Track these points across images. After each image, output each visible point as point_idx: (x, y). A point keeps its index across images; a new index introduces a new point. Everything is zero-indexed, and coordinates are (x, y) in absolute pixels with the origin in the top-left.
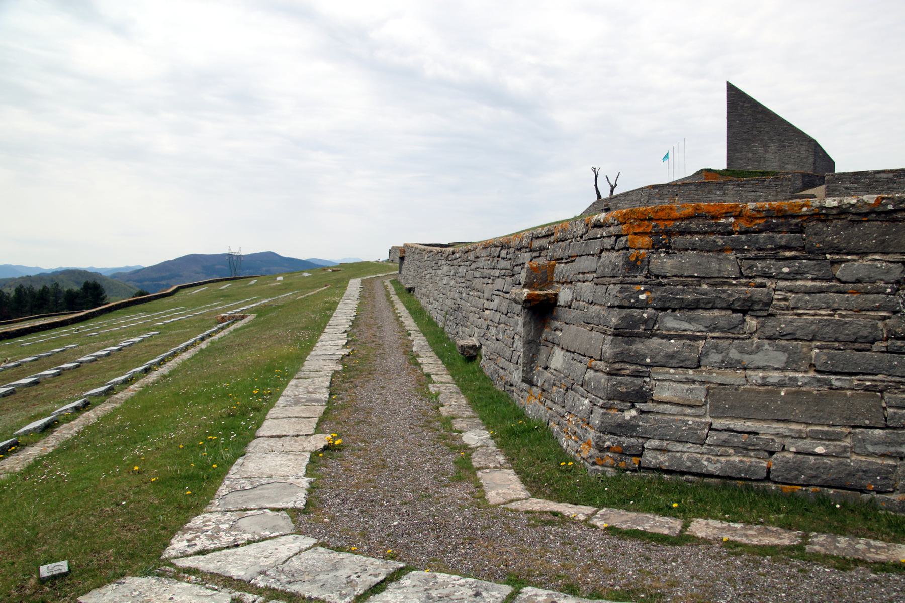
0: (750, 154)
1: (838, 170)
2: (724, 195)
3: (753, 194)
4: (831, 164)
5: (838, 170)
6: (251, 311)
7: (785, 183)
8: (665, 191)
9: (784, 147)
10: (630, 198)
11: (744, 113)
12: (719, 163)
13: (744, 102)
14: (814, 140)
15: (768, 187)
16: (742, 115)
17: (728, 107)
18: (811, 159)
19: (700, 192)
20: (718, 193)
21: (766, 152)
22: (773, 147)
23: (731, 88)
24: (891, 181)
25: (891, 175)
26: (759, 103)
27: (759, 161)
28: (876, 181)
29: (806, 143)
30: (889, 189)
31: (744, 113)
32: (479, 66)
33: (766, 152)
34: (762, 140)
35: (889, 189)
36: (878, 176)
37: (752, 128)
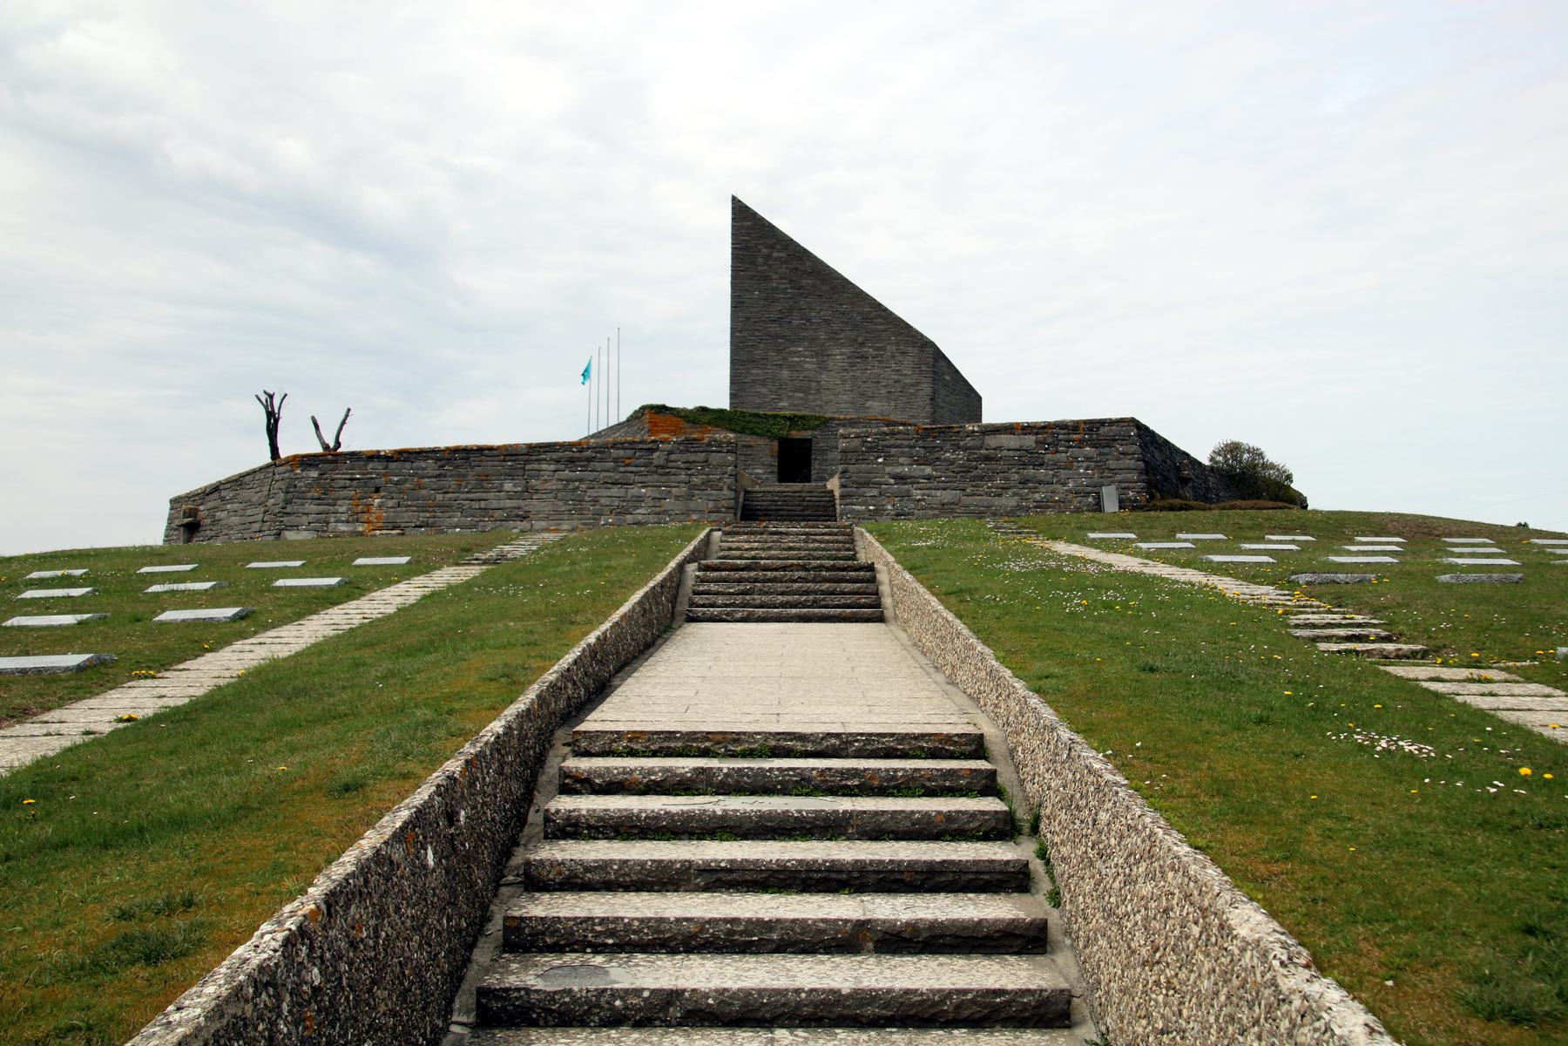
0: (785, 373)
1: (991, 414)
2: (528, 491)
3: (615, 491)
4: (971, 401)
5: (991, 414)
6: (1093, 544)
7: (715, 458)
8: (341, 475)
9: (864, 357)
10: (245, 494)
11: (772, 273)
12: (709, 387)
13: (772, 247)
14: (932, 344)
15: (664, 469)
16: (767, 278)
17: (735, 257)
18: (926, 388)
19: (451, 483)
20: (508, 486)
21: (822, 367)
22: (839, 355)
23: (742, 215)
24: (1029, 459)
25: (1029, 441)
26: (806, 251)
27: (806, 391)
28: (988, 459)
29: (913, 351)
30: (1024, 482)
31: (772, 273)
32: (295, 153)
33: (822, 367)
34: (813, 340)
35: (1024, 482)
36: (992, 441)
37: (790, 310)
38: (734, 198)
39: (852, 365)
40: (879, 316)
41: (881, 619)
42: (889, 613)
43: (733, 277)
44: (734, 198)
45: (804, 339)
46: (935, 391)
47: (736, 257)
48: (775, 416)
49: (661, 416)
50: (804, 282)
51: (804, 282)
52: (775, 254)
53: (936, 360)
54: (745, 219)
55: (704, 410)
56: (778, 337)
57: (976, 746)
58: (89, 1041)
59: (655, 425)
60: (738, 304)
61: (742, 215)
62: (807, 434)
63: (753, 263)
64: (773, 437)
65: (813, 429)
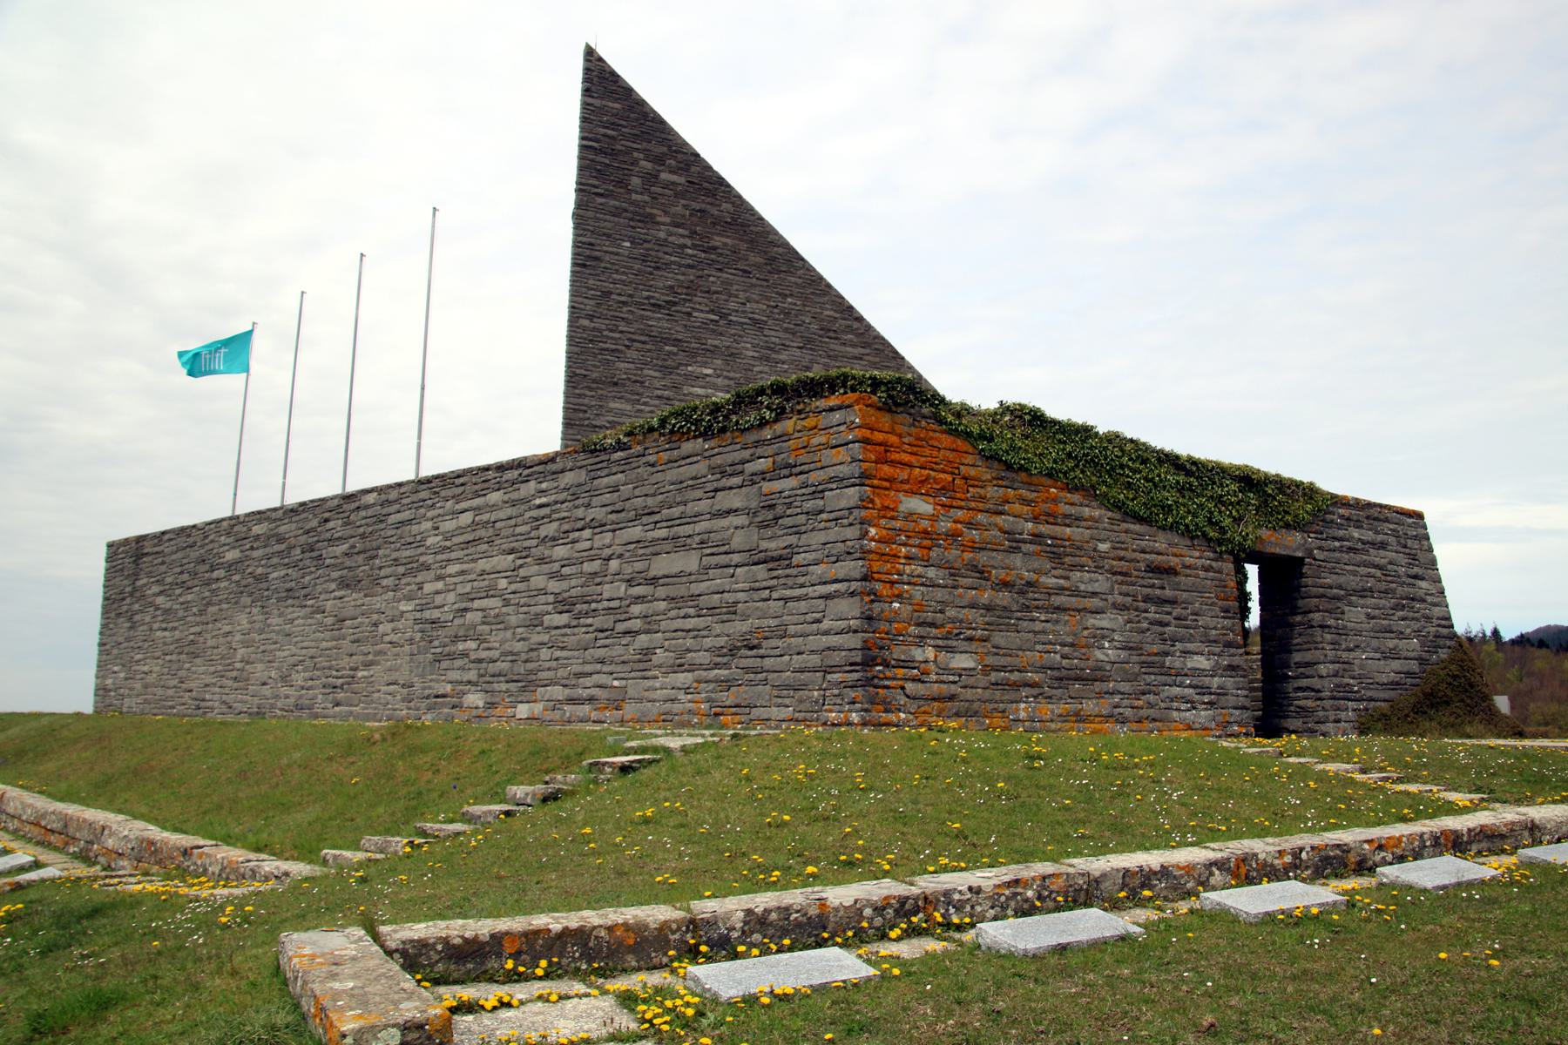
26: (721, 182)
31: (645, 195)
34: (732, 356)
37: (691, 288)
38: (590, 53)
40: (849, 329)
44: (590, 53)
45: (714, 351)
50: (718, 241)
52: (664, 176)
56: (666, 341)
58: (191, 1044)
59: (884, 454)
60: (585, 261)
63: (622, 183)
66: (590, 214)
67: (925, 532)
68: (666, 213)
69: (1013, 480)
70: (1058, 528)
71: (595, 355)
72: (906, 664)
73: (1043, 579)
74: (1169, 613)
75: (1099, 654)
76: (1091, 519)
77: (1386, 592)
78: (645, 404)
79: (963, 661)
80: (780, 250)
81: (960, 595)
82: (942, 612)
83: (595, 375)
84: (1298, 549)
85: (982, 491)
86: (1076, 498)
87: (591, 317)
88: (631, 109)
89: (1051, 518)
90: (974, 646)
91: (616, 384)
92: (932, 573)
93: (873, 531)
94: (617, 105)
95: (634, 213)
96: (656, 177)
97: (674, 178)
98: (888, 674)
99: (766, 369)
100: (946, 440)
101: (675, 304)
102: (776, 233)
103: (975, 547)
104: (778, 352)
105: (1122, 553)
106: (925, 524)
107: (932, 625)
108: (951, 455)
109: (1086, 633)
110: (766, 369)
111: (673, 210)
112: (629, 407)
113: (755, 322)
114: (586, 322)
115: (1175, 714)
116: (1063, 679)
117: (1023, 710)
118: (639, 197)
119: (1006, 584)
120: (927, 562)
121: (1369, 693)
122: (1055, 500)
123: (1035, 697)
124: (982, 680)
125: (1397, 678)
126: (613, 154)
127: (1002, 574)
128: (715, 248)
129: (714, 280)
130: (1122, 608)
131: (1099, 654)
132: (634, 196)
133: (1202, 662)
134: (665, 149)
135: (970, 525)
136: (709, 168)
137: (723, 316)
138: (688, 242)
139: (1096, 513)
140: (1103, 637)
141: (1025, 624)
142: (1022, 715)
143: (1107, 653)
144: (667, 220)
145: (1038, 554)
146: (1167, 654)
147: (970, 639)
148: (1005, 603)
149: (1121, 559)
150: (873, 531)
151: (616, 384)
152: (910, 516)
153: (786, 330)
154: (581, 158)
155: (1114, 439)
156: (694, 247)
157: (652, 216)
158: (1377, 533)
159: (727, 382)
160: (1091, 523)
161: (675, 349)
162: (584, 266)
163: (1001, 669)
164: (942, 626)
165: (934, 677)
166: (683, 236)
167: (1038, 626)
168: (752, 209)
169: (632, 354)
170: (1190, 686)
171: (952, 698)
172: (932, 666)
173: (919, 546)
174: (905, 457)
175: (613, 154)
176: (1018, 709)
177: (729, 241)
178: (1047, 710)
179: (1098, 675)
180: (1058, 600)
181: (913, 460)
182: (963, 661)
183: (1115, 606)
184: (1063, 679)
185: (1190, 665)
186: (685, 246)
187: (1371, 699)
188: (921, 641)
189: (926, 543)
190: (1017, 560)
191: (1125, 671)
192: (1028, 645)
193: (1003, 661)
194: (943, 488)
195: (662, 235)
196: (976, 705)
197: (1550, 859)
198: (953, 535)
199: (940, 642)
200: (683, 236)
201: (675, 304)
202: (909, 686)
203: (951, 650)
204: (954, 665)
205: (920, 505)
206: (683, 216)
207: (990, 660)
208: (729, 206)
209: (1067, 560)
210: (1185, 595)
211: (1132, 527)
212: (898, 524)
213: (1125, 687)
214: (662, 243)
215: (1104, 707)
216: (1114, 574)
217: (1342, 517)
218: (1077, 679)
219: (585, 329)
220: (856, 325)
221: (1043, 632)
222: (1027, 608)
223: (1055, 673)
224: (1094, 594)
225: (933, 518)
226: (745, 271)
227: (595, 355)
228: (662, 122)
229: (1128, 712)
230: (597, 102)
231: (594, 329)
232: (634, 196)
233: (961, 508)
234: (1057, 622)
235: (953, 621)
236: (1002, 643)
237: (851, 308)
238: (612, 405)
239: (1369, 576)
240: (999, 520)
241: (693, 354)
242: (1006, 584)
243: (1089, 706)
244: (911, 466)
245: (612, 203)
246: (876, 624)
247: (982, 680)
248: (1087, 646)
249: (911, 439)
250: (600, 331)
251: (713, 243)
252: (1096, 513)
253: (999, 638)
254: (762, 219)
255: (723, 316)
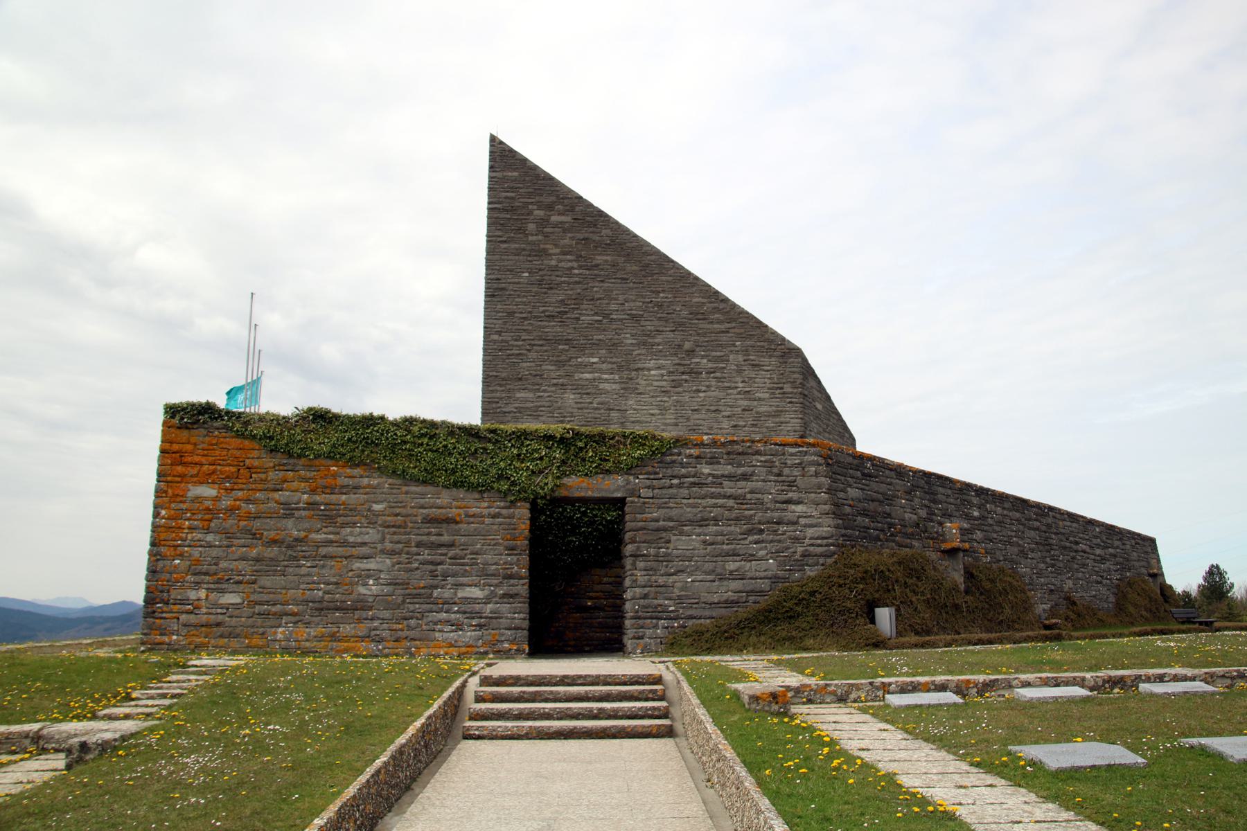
0: (570, 397)
9: (694, 373)
14: (797, 352)
17: (493, 223)
21: (629, 388)
22: (655, 371)
23: (505, 163)
26: (601, 214)
29: (770, 362)
33: (629, 388)
34: (614, 346)
37: (579, 299)
39: (676, 384)
40: (716, 310)
41: (669, 733)
42: (679, 727)
43: (490, 252)
45: (599, 344)
46: (805, 425)
47: (494, 222)
48: (522, 436)
49: (198, 435)
50: (599, 259)
51: (599, 259)
52: (555, 218)
53: (805, 378)
54: (509, 167)
55: (320, 418)
56: (559, 342)
57: (658, 680)
60: (494, 291)
61: (505, 163)
62: (612, 486)
63: (522, 230)
64: (514, 494)
65: (630, 470)
66: (497, 257)
67: (208, 509)
68: (556, 246)
69: (295, 465)
70: (333, 496)
71: (504, 360)
72: (184, 602)
73: (313, 536)
74: (445, 555)
75: (362, 590)
76: (369, 486)
77: (737, 519)
78: (544, 391)
79: (231, 599)
80: (653, 257)
81: (233, 552)
82: (216, 564)
83: (504, 375)
84: (617, 490)
85: (263, 476)
86: (357, 471)
87: (499, 333)
88: (526, 174)
89: (331, 490)
90: (242, 587)
91: (520, 379)
92: (210, 537)
93: (163, 512)
94: (515, 174)
95: (531, 250)
96: (548, 221)
97: (563, 218)
98: (165, 609)
99: (644, 352)
100: (236, 442)
101: (566, 313)
102: (649, 245)
103: (250, 517)
104: (653, 337)
105: (398, 511)
106: (209, 504)
107: (206, 574)
108: (238, 453)
109: (350, 574)
110: (644, 352)
111: (562, 242)
112: (531, 395)
113: (633, 316)
114: (496, 337)
115: (437, 634)
116: (322, 608)
117: (280, 633)
118: (534, 238)
119: (274, 542)
120: (208, 530)
121: (689, 612)
122: (335, 476)
123: (295, 623)
124: (247, 611)
125: (734, 597)
126: (513, 209)
127: (272, 534)
128: (597, 266)
129: (597, 289)
130: (392, 553)
131: (362, 590)
132: (530, 238)
133: (476, 593)
134: (554, 198)
135: (248, 501)
136: (591, 205)
137: (606, 316)
138: (575, 265)
139: (375, 482)
140: (369, 577)
141: (291, 570)
142: (279, 636)
143: (371, 588)
144: (558, 251)
145: (310, 517)
146: (436, 587)
147: (239, 582)
148: (272, 555)
149: (397, 515)
150: (163, 512)
151: (520, 379)
152: (197, 499)
153: (660, 319)
154: (489, 218)
155: (409, 422)
156: (580, 267)
157: (545, 250)
158: (740, 465)
159: (610, 366)
160: (375, 492)
161: (566, 347)
162: (493, 296)
163: (267, 603)
164: (215, 574)
165: (204, 610)
166: (570, 261)
167: (304, 571)
168: (628, 230)
169: (532, 355)
170: (458, 612)
171: (218, 624)
172: (203, 603)
173: (201, 520)
174: (196, 459)
175: (513, 209)
176: (275, 633)
177: (609, 258)
178: (303, 632)
179: (361, 605)
180: (323, 551)
181: (204, 460)
182: (231, 599)
183: (383, 551)
184: (322, 608)
185: (460, 594)
186: (573, 268)
187: (691, 617)
188: (197, 585)
189: (207, 517)
190: (290, 523)
191: (388, 603)
192: (292, 585)
193: (266, 597)
194: (228, 477)
195: (553, 263)
196: (238, 630)
197: (1221, 749)
198: (231, 510)
199: (212, 586)
200: (570, 261)
201: (566, 313)
202: (183, 617)
203: (223, 591)
204: (221, 601)
205: (208, 491)
206: (571, 246)
207: (254, 597)
208: (608, 232)
209: (339, 520)
210: (463, 539)
211: (413, 489)
212: (184, 506)
213: (386, 614)
214: (553, 269)
215: (362, 629)
216: (388, 527)
217: (690, 456)
218: (337, 609)
219: (495, 342)
220: (722, 306)
221: (309, 575)
222: (296, 559)
223: (316, 605)
224: (364, 544)
225: (216, 499)
226: (623, 279)
227: (504, 360)
228: (552, 179)
229: (386, 634)
230: (499, 175)
231: (502, 341)
232: (530, 238)
233: (242, 490)
234: (323, 566)
235: (225, 570)
236: (268, 584)
237: (717, 293)
238: (518, 395)
239: (715, 506)
240: (276, 495)
241: (582, 349)
242: (274, 542)
243: (346, 629)
244: (202, 465)
245: (513, 246)
246: (157, 576)
247: (247, 611)
248: (351, 584)
249: (205, 446)
250: (507, 342)
251: (595, 262)
252: (375, 482)
253: (266, 581)
254: (636, 236)
255: (606, 316)
